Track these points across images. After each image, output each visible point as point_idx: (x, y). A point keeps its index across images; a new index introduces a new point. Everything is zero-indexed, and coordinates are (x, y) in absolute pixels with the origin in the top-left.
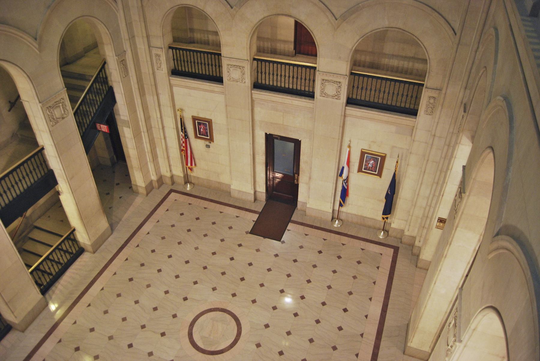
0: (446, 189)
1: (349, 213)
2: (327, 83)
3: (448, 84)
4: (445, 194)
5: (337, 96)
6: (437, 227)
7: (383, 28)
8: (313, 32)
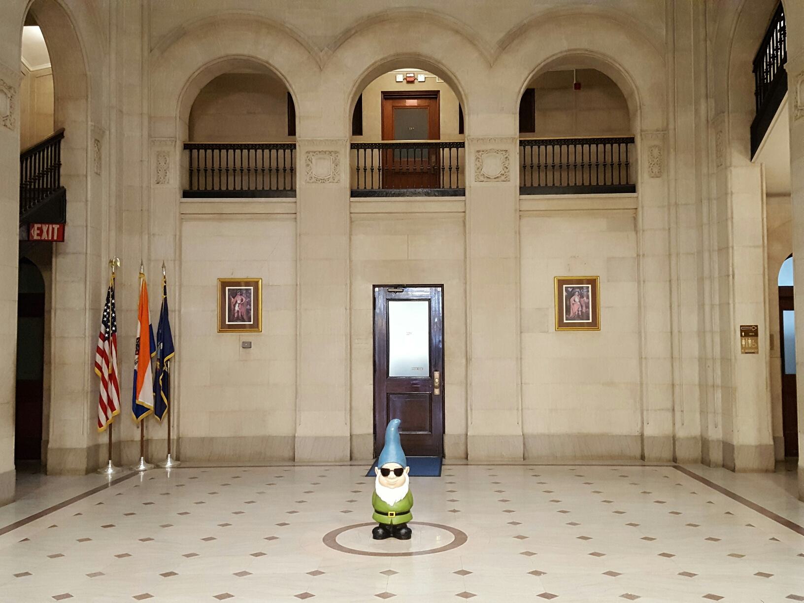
0: (735, 261)
1: (553, 436)
2: (485, 155)
3: (674, 106)
4: (736, 272)
5: (503, 177)
6: (746, 351)
7: (561, 52)
8: (457, 74)
